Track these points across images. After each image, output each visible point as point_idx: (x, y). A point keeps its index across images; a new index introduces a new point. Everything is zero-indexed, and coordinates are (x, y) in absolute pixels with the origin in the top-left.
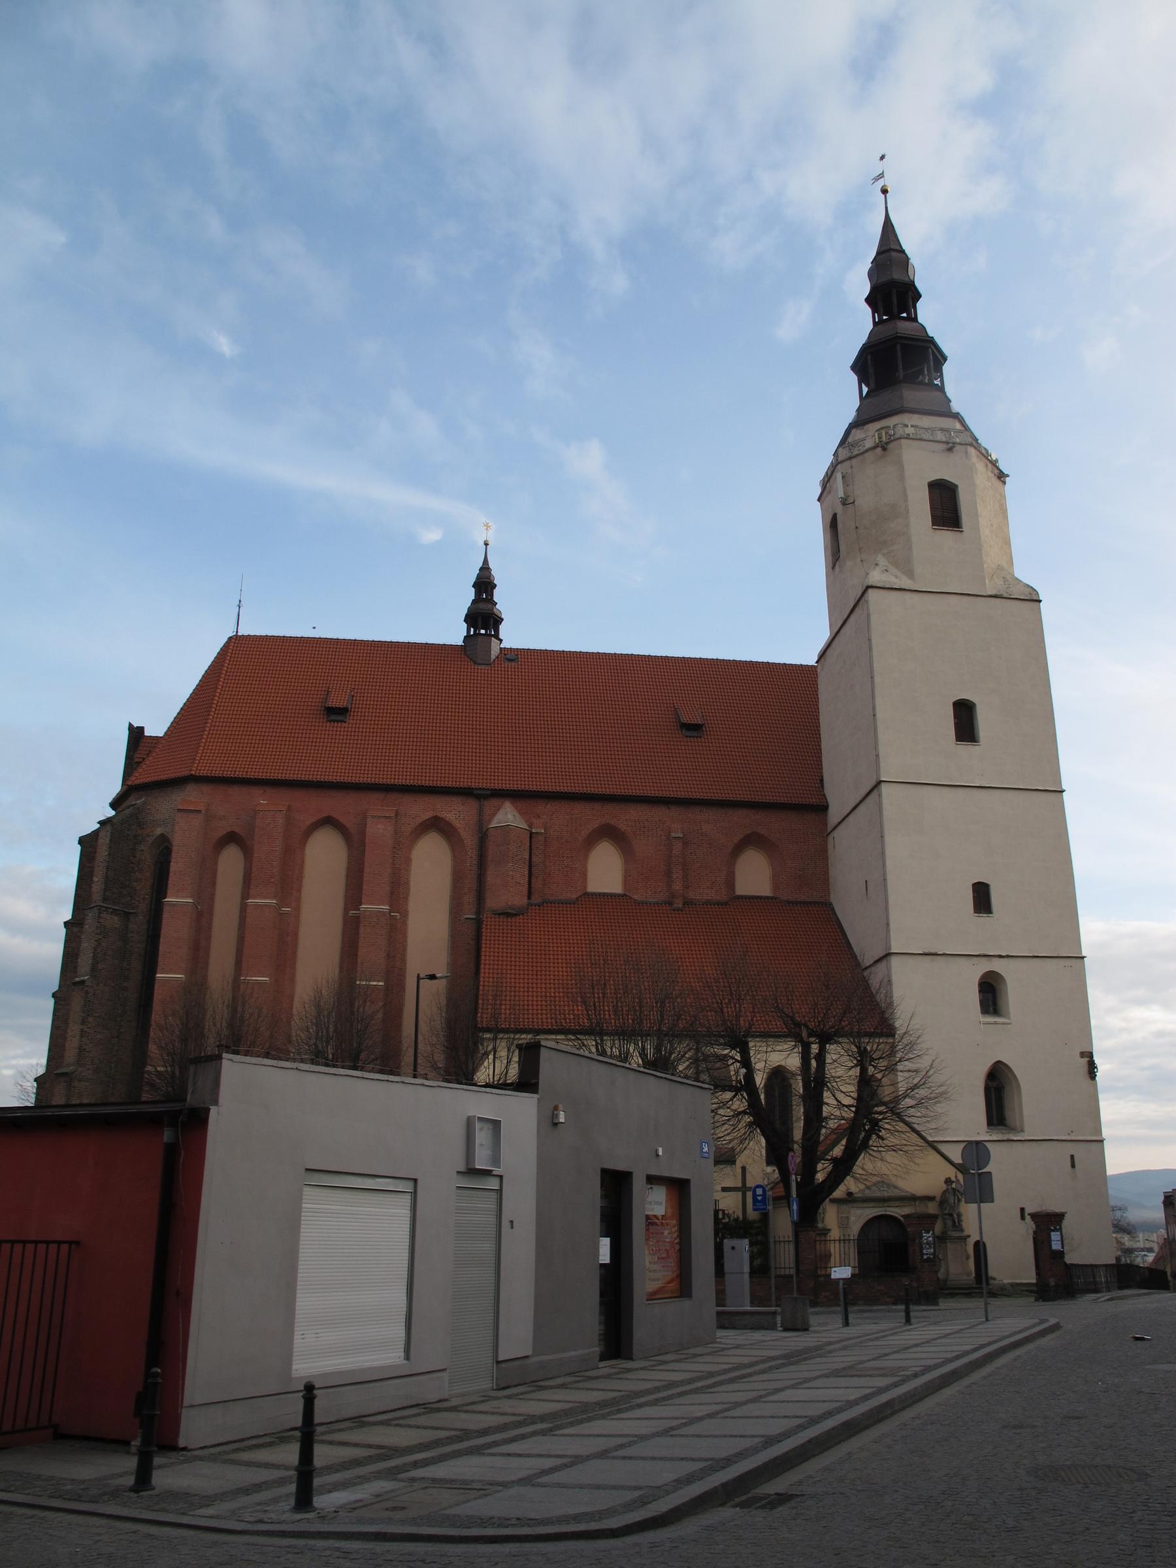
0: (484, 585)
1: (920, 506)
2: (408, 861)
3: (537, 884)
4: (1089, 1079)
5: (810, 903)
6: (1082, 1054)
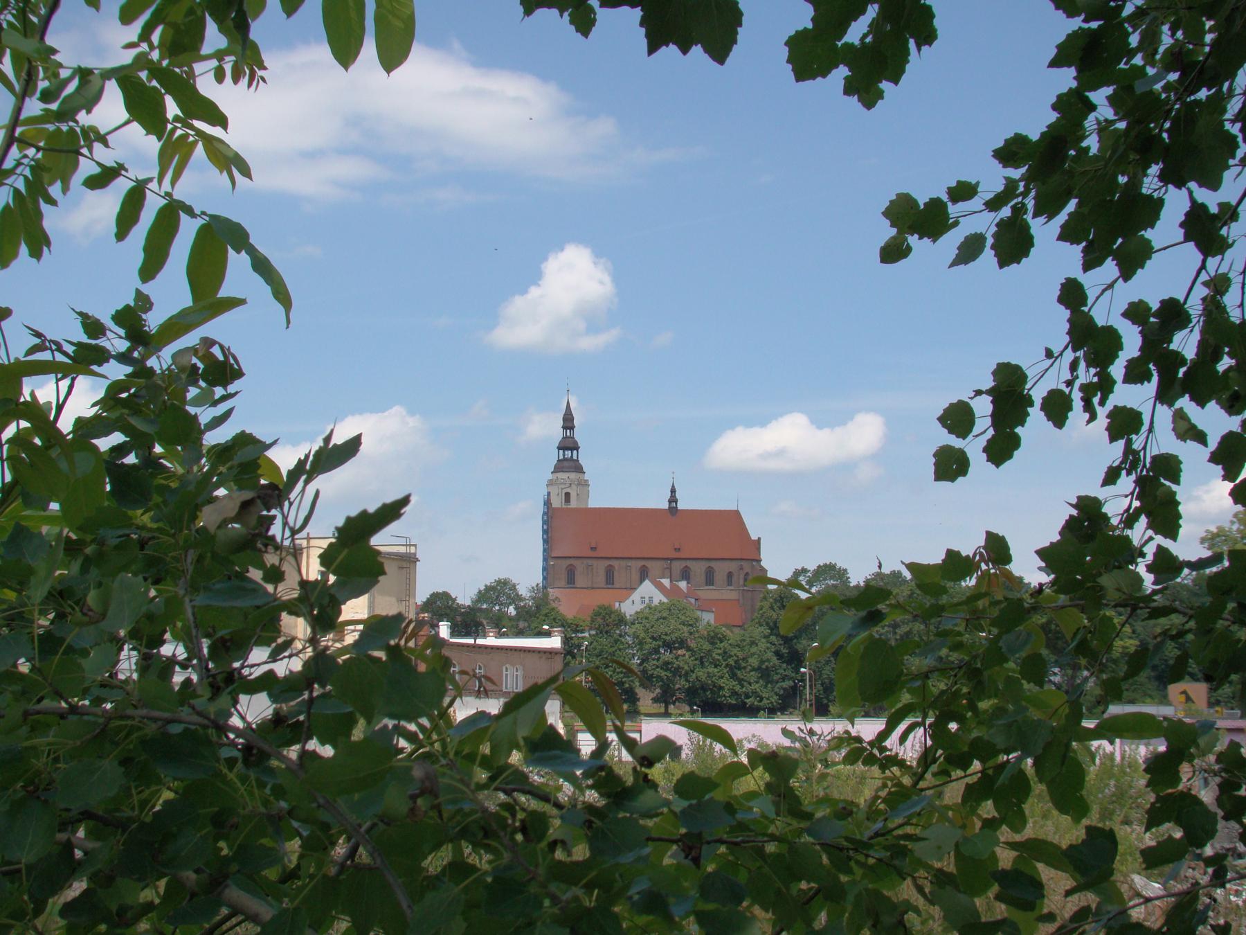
0: (673, 491)
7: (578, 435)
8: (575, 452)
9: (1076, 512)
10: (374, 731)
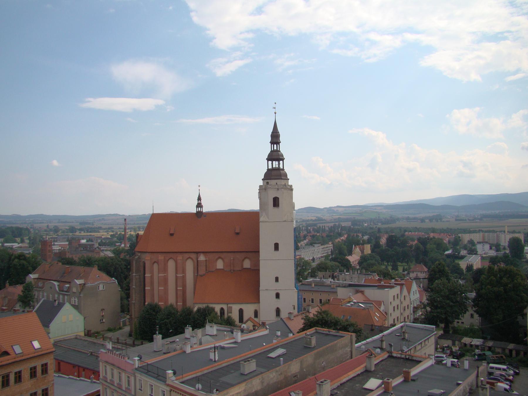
0: (199, 199)
2: (185, 265)
7: (283, 148)
8: (281, 162)
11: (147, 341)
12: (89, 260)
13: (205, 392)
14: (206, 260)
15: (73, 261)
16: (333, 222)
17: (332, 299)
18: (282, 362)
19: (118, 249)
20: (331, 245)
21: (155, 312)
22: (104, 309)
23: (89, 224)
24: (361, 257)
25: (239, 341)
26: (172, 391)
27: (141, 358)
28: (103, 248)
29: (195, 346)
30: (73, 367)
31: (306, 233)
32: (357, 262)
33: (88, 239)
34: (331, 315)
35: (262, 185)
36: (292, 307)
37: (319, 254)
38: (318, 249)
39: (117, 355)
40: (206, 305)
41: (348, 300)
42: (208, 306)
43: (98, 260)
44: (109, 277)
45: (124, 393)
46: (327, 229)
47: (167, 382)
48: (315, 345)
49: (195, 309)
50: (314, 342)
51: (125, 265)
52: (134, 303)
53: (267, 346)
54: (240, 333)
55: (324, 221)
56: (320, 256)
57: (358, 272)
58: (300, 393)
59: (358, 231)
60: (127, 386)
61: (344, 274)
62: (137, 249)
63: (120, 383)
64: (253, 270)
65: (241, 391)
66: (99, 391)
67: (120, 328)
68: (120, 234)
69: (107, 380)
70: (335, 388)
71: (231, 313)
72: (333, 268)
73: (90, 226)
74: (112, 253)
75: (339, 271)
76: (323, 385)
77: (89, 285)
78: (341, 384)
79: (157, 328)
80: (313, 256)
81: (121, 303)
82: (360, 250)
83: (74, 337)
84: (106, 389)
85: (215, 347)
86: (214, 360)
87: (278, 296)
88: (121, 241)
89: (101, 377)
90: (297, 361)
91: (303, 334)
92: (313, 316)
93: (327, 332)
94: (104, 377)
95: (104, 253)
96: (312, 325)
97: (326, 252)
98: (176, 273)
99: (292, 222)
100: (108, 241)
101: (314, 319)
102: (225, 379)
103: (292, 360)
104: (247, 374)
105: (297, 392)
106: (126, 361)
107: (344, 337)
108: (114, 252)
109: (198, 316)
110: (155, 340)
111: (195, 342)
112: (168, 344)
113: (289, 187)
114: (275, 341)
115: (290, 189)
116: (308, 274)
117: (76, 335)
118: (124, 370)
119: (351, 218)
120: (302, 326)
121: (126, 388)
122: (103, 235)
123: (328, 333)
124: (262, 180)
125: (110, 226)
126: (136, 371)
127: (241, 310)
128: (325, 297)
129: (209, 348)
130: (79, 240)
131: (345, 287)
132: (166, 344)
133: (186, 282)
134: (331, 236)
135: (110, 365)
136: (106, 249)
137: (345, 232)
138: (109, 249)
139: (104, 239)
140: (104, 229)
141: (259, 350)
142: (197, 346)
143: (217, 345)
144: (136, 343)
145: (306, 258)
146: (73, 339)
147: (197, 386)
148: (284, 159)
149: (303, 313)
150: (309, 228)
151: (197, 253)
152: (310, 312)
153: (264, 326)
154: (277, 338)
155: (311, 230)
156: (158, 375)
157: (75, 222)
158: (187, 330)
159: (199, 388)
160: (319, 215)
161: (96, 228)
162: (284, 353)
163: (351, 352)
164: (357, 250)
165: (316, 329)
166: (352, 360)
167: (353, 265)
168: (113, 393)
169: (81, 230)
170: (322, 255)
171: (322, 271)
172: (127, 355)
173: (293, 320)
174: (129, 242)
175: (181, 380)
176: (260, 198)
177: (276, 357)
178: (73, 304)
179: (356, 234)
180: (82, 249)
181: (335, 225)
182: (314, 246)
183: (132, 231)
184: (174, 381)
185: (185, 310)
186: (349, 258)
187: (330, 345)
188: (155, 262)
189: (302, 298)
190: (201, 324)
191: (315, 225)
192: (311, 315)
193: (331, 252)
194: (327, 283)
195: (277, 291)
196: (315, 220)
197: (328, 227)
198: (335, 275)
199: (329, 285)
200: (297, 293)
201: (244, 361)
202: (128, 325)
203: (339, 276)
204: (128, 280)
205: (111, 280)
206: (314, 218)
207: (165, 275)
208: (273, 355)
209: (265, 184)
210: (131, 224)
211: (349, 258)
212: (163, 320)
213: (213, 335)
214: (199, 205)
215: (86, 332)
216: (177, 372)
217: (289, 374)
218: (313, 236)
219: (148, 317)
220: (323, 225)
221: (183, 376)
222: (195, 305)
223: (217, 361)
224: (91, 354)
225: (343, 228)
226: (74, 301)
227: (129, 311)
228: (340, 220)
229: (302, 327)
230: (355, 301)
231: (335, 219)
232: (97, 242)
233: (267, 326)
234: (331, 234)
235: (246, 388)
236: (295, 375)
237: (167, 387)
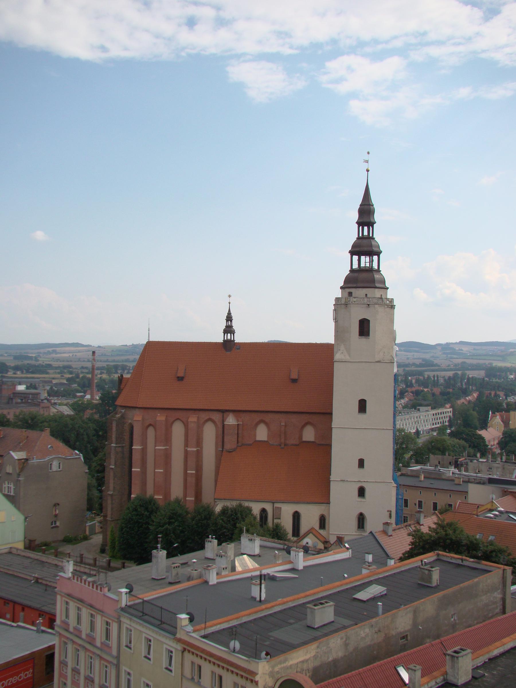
0: (229, 318)
1: (355, 328)
2: (202, 431)
3: (240, 439)
4: (389, 517)
5: (325, 445)
6: (388, 511)
8: (375, 258)
9: (264, 599)
10: (260, 566)
11: (132, 561)
12: (32, 419)
13: (246, 657)
14: (238, 424)
15: (5, 420)
16: (451, 370)
17: (458, 503)
18: (380, 610)
19: (80, 402)
20: (449, 410)
21: (148, 511)
22: (58, 504)
23: (31, 358)
24: (504, 433)
25: (301, 567)
26: (186, 652)
27: (131, 589)
28: (54, 400)
29: (224, 573)
30: (5, 602)
31: (404, 386)
32: (496, 442)
33: (29, 385)
34: (462, 531)
35: (340, 297)
36: (387, 513)
37: (428, 425)
38: (425, 416)
39: (89, 583)
40: (238, 502)
41: (489, 506)
42: (240, 505)
43: (47, 420)
44: (70, 449)
45: (98, 652)
46: (441, 381)
47: (178, 636)
48: (438, 584)
49: (218, 509)
50: (436, 576)
51: (95, 430)
52: (112, 495)
53: (352, 579)
54: (302, 553)
55: (437, 368)
56: (429, 428)
57: (501, 459)
58: (418, 670)
59: (498, 387)
60: (104, 639)
61: (477, 460)
62: (119, 402)
63: (92, 633)
64: (318, 444)
65: (310, 658)
66: (52, 647)
67: (86, 538)
68: (84, 377)
69: (69, 628)
70: (480, 666)
71: (280, 519)
72: (456, 449)
73: (33, 362)
74: (70, 409)
75: (469, 456)
76: (460, 659)
77: (35, 461)
78: (490, 659)
79: (159, 537)
80: (417, 427)
81: (88, 494)
82: (502, 421)
83: (6, 551)
84: (66, 643)
85: (261, 576)
86: (258, 599)
87: (361, 492)
88: (85, 389)
89: (58, 622)
90: (408, 610)
91: (415, 562)
92: (428, 531)
93: (458, 560)
94: (63, 622)
95: (58, 410)
96: (427, 546)
97: (439, 421)
98: (186, 445)
99: (392, 364)
100: (62, 389)
101: (431, 536)
102: (280, 634)
103: (397, 607)
104: (318, 628)
105: (411, 666)
106: (104, 595)
107: (490, 571)
108: (75, 407)
109: (224, 521)
110: (154, 560)
111: (224, 566)
112: (177, 567)
113: (388, 302)
114: (365, 571)
115: (390, 306)
116: (411, 458)
117: (11, 548)
118: (101, 612)
119: (485, 364)
120: (408, 548)
121: (102, 643)
122: (53, 378)
123: (460, 562)
124: (341, 288)
125: (66, 364)
126: (123, 613)
127: (296, 514)
128: (442, 500)
129: (248, 578)
130: (14, 385)
131: (479, 483)
132: (174, 568)
133: (202, 461)
134: (448, 393)
135: (76, 601)
136: (60, 401)
137: (474, 388)
138: (65, 402)
139: (56, 384)
140: (56, 368)
141: (338, 586)
142: (227, 573)
143: (264, 572)
144: (112, 564)
145: (408, 430)
146: (6, 553)
147: (232, 644)
148: (381, 252)
149: (410, 525)
150: (410, 378)
151: (224, 412)
152: (421, 523)
153: (342, 544)
154: (369, 566)
155: (414, 381)
156: (161, 621)
157: (6, 355)
158: (210, 543)
159: (234, 648)
160: (427, 356)
161: (43, 365)
162: (382, 594)
163: (504, 600)
164: (496, 420)
165: (438, 555)
166: (504, 616)
167: (489, 447)
168: (78, 651)
169: (16, 368)
170: (433, 427)
171: (436, 454)
172: (106, 583)
173: (391, 536)
174: (98, 391)
175: (203, 633)
176: (336, 320)
177: (368, 600)
178: (6, 493)
179: (494, 392)
180: (19, 401)
181: (456, 374)
182: (419, 410)
183: (103, 373)
184: (191, 634)
185: (201, 510)
186: (482, 433)
187: (466, 584)
188: (150, 425)
189: (402, 499)
190: (227, 535)
191: (421, 373)
192: (425, 530)
193: (450, 421)
194: (447, 475)
195: (360, 485)
196: (421, 365)
197: (443, 378)
198: (461, 462)
199: (450, 478)
200: (395, 489)
201: (313, 604)
202: (98, 533)
203: (467, 464)
204: (100, 455)
205: (73, 454)
206: (418, 362)
207: (166, 449)
208: (363, 595)
209: (346, 295)
210: (101, 361)
211: (482, 433)
212: (163, 526)
213: (254, 556)
214: (229, 330)
215: (27, 542)
216: (195, 620)
217: (393, 633)
218: (417, 393)
219: (136, 520)
220: (436, 373)
221: (206, 626)
222: (218, 503)
223: (263, 601)
224: (37, 581)
225: (471, 381)
226: (8, 489)
227: (101, 509)
228: (464, 367)
229: (408, 550)
230: (502, 509)
231: (456, 365)
232: (45, 390)
233: (347, 545)
234: (448, 390)
235: (317, 652)
236: (402, 636)
237: (177, 644)
